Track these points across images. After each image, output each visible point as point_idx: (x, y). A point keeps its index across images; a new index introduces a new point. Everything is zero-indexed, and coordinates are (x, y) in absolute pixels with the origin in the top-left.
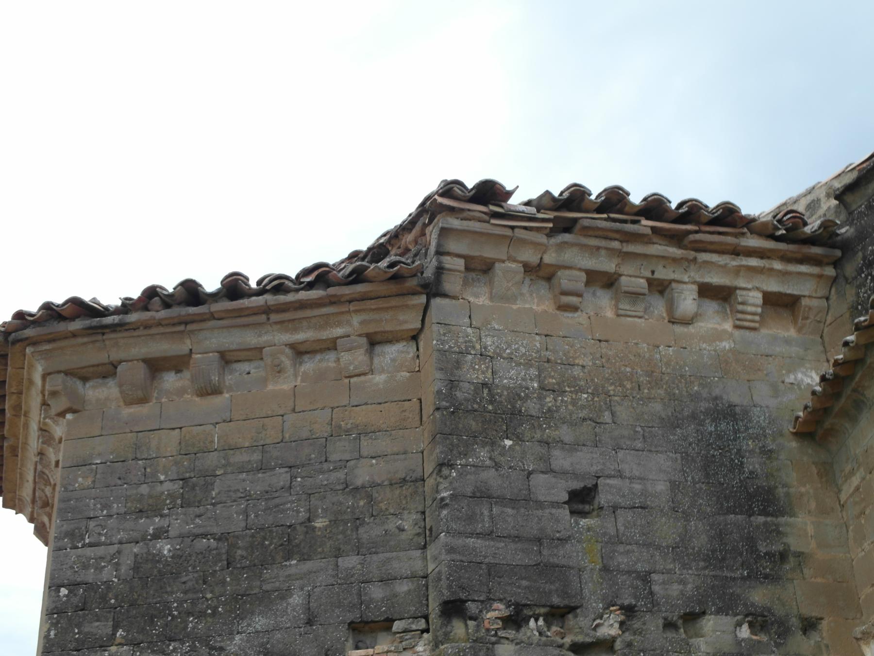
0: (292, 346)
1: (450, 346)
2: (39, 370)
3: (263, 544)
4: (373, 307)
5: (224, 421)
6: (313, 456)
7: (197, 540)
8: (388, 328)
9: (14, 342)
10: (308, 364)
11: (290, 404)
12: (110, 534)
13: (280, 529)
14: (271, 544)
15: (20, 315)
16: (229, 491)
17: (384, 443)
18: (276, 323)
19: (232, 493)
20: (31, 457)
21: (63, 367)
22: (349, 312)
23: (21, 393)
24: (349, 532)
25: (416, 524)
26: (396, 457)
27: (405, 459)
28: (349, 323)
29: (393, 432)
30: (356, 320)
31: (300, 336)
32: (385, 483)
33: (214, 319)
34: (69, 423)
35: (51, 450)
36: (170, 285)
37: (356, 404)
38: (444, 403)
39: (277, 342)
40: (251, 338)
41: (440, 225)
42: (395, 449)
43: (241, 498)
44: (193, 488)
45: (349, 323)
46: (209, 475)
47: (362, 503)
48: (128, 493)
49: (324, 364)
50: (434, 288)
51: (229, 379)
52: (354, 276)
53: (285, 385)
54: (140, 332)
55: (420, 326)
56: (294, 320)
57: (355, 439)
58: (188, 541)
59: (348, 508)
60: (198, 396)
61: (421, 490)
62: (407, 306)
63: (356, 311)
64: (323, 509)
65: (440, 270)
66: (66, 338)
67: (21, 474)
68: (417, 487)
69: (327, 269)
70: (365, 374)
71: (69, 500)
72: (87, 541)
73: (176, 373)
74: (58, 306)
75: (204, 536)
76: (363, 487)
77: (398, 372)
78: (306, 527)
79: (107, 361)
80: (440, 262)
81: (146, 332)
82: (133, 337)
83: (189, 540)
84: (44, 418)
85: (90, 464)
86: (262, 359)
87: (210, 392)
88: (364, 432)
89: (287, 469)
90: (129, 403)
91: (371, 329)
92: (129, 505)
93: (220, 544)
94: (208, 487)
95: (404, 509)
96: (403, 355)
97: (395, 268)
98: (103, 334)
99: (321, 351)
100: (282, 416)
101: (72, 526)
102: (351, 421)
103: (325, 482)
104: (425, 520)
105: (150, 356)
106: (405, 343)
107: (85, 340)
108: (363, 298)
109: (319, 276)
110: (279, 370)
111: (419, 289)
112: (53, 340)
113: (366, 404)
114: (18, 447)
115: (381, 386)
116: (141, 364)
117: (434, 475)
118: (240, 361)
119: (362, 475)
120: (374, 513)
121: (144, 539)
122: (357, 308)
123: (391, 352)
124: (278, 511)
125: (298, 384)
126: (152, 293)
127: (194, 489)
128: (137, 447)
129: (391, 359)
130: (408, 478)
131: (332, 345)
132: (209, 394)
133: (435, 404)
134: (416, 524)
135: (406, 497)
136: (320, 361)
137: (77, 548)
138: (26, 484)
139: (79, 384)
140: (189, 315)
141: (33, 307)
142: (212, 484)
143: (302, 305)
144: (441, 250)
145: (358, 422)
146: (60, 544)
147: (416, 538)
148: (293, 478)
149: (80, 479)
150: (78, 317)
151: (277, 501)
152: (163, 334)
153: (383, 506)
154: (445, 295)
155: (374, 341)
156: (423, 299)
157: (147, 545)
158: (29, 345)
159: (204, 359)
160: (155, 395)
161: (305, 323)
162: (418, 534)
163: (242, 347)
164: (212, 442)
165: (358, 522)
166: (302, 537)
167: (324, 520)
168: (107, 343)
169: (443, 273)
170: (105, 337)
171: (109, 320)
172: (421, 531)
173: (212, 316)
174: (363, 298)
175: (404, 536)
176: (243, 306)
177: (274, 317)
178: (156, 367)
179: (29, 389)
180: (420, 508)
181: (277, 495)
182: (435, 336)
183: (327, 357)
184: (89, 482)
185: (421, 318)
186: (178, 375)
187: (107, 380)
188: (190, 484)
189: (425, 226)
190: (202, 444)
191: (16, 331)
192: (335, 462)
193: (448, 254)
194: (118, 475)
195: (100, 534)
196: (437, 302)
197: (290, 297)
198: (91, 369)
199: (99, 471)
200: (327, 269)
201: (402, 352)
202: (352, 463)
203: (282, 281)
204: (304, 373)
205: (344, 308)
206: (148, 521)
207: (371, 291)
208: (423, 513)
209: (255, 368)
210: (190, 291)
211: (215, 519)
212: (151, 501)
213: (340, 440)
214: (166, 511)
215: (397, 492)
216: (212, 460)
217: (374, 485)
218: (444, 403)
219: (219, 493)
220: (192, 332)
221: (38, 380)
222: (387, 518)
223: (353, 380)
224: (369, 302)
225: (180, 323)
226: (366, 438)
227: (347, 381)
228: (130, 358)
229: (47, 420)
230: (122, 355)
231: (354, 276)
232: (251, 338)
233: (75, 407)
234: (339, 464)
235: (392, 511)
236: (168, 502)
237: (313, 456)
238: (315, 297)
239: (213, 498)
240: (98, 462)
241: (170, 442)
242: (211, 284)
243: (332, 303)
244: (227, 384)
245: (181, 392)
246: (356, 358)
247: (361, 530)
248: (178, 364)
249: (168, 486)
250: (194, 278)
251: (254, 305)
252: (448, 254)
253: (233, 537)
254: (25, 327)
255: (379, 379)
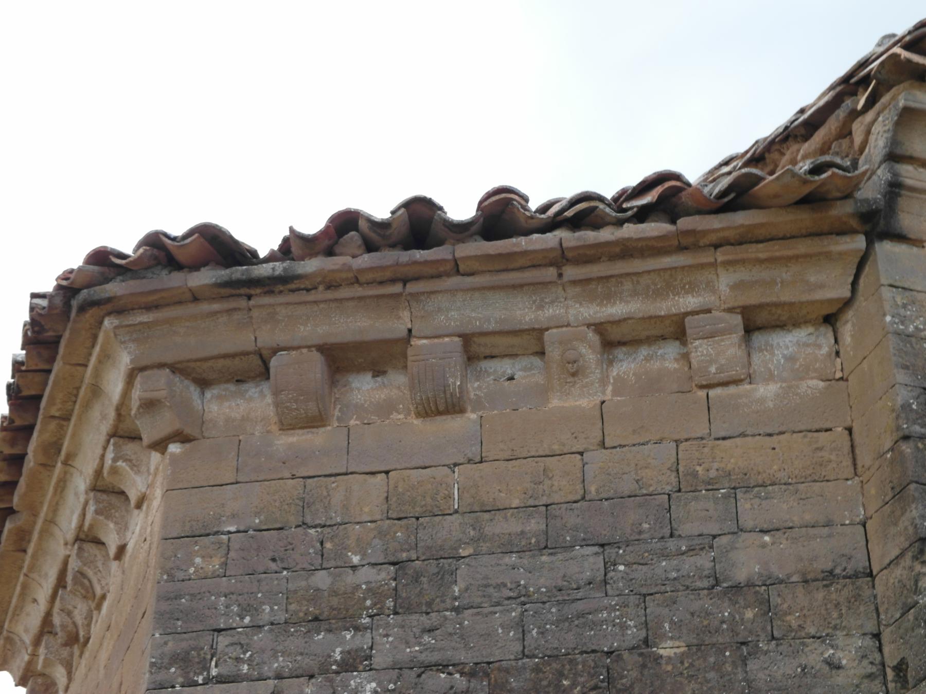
0: (599, 327)
1: (916, 328)
2: (125, 360)
3: (558, 686)
4: (762, 256)
5: (470, 461)
6: (646, 526)
7: (429, 673)
8: (786, 296)
9: (82, 309)
10: (625, 364)
11: (597, 435)
12: (257, 660)
13: (590, 658)
14: (574, 685)
15: (101, 258)
16: (487, 586)
17: (785, 506)
18: (574, 283)
19: (491, 590)
20: (59, 548)
21: (169, 358)
22: (714, 265)
23: (67, 418)
24: (728, 668)
25: (864, 657)
26: (812, 531)
27: (830, 536)
28: (710, 287)
29: (801, 487)
30: (725, 281)
31: (616, 310)
32: (795, 578)
33: (458, 272)
34: (174, 459)
35: (112, 525)
36: (380, 207)
37: (723, 434)
38: (917, 428)
39: (571, 319)
40: (523, 311)
41: (901, 103)
42: (808, 517)
43: (509, 598)
44: (416, 579)
45: (710, 287)
46: (446, 559)
47: (749, 614)
48: (291, 586)
49: (656, 365)
50: (882, 222)
51: (474, 388)
52: (732, 196)
53: (583, 401)
54: (320, 294)
55: (848, 294)
56: (608, 278)
57: (725, 497)
58: (410, 675)
59: (723, 622)
60: (418, 415)
61: (867, 592)
62: (828, 256)
63: (728, 264)
64: (672, 622)
65: (895, 188)
66: (180, 303)
67: (25, 587)
68: (859, 588)
69: (678, 184)
70: (737, 382)
71: (178, 597)
72: (214, 672)
73: (373, 377)
74: (174, 239)
75: (442, 666)
76: (750, 585)
77: (802, 379)
78: (641, 655)
79: (251, 347)
80: (895, 175)
81: (330, 295)
82: (305, 303)
83: (413, 673)
84: (115, 460)
85: (216, 533)
86: (541, 353)
87: (441, 408)
88: (742, 485)
89: (596, 549)
90: (287, 426)
91: (752, 298)
92: (293, 607)
93: (474, 683)
94: (445, 578)
95: (835, 628)
96: (809, 350)
97: (824, 176)
98: (249, 297)
99: (650, 340)
100: (581, 454)
101: (184, 645)
102: (716, 465)
103: (674, 575)
104: (880, 649)
105: (332, 340)
106: (811, 329)
107: (216, 306)
108: (744, 239)
109: (663, 196)
110: (574, 371)
111: (854, 223)
112: (156, 307)
113: (743, 435)
114: (30, 533)
115: (771, 404)
116: (317, 356)
117: (907, 561)
118: (493, 357)
119: (747, 561)
120: (776, 634)
121: (324, 670)
122: (730, 257)
123: (786, 343)
124: (585, 624)
125: (608, 396)
126: (346, 223)
127: (416, 580)
128: (305, 505)
129: (784, 356)
130: (838, 571)
131: (677, 330)
132: (440, 413)
133: (898, 428)
134: (864, 657)
135: (837, 605)
136: (648, 359)
137: (196, 684)
138: (29, 607)
139: (193, 391)
140: (416, 263)
141: (126, 243)
142: (453, 573)
143: (627, 251)
144: (899, 151)
145: (730, 467)
146: (161, 676)
147: (865, 685)
148: (609, 565)
149: (198, 560)
150: (205, 264)
151: (580, 606)
152: (361, 298)
153: (792, 620)
154: (900, 237)
155: (755, 323)
156: (860, 242)
157: (331, 681)
158: (109, 314)
159: (435, 350)
160: (337, 413)
161: (628, 285)
162: (870, 676)
163: (507, 328)
164: (450, 496)
165: (745, 648)
166: (634, 674)
167: (677, 643)
168: (255, 313)
169: (899, 195)
170: (252, 302)
171: (264, 270)
172: (874, 669)
173: (456, 269)
174: (744, 239)
175: (840, 679)
176: (516, 249)
177: (571, 272)
178: (341, 360)
179: (87, 406)
180: (871, 627)
181: (579, 596)
182: (887, 307)
183: (660, 352)
184: (215, 564)
185: (851, 279)
186: (379, 379)
187: (245, 386)
188: (410, 572)
189: (855, 114)
190: (428, 500)
191: (89, 286)
192: (690, 537)
193: (910, 159)
194: (271, 554)
195: (238, 659)
196: (885, 248)
197: (606, 234)
198: (221, 363)
199: (235, 545)
200: (678, 184)
201: (807, 345)
202: (724, 540)
203: (593, 204)
204: (618, 379)
205: (706, 257)
206: (330, 636)
207: (762, 225)
208: (877, 636)
209: (525, 369)
210: (420, 222)
211: (462, 637)
212: (335, 601)
213: (696, 499)
214: (366, 621)
215: (820, 595)
216: (449, 529)
217: (771, 582)
218: (917, 428)
219: (467, 589)
220: (415, 296)
221: (114, 385)
222: (804, 644)
223: (712, 393)
224: (753, 247)
225: (393, 281)
226: (748, 496)
227: (702, 393)
228: (296, 344)
229: (120, 463)
230: (281, 337)
231: (732, 196)
232: (523, 311)
233: (188, 431)
234: (697, 541)
235: (812, 631)
236: (368, 603)
237: (646, 526)
238: (655, 234)
239: (456, 599)
240: (233, 529)
241: (367, 497)
242: (461, 207)
243: (682, 248)
244: (472, 396)
245: (386, 409)
246: (717, 351)
247: (752, 665)
248: (380, 357)
249: (367, 575)
250: (428, 195)
251: (538, 247)
252: (910, 159)
253: (499, 669)
254: (107, 280)
255: (766, 391)
